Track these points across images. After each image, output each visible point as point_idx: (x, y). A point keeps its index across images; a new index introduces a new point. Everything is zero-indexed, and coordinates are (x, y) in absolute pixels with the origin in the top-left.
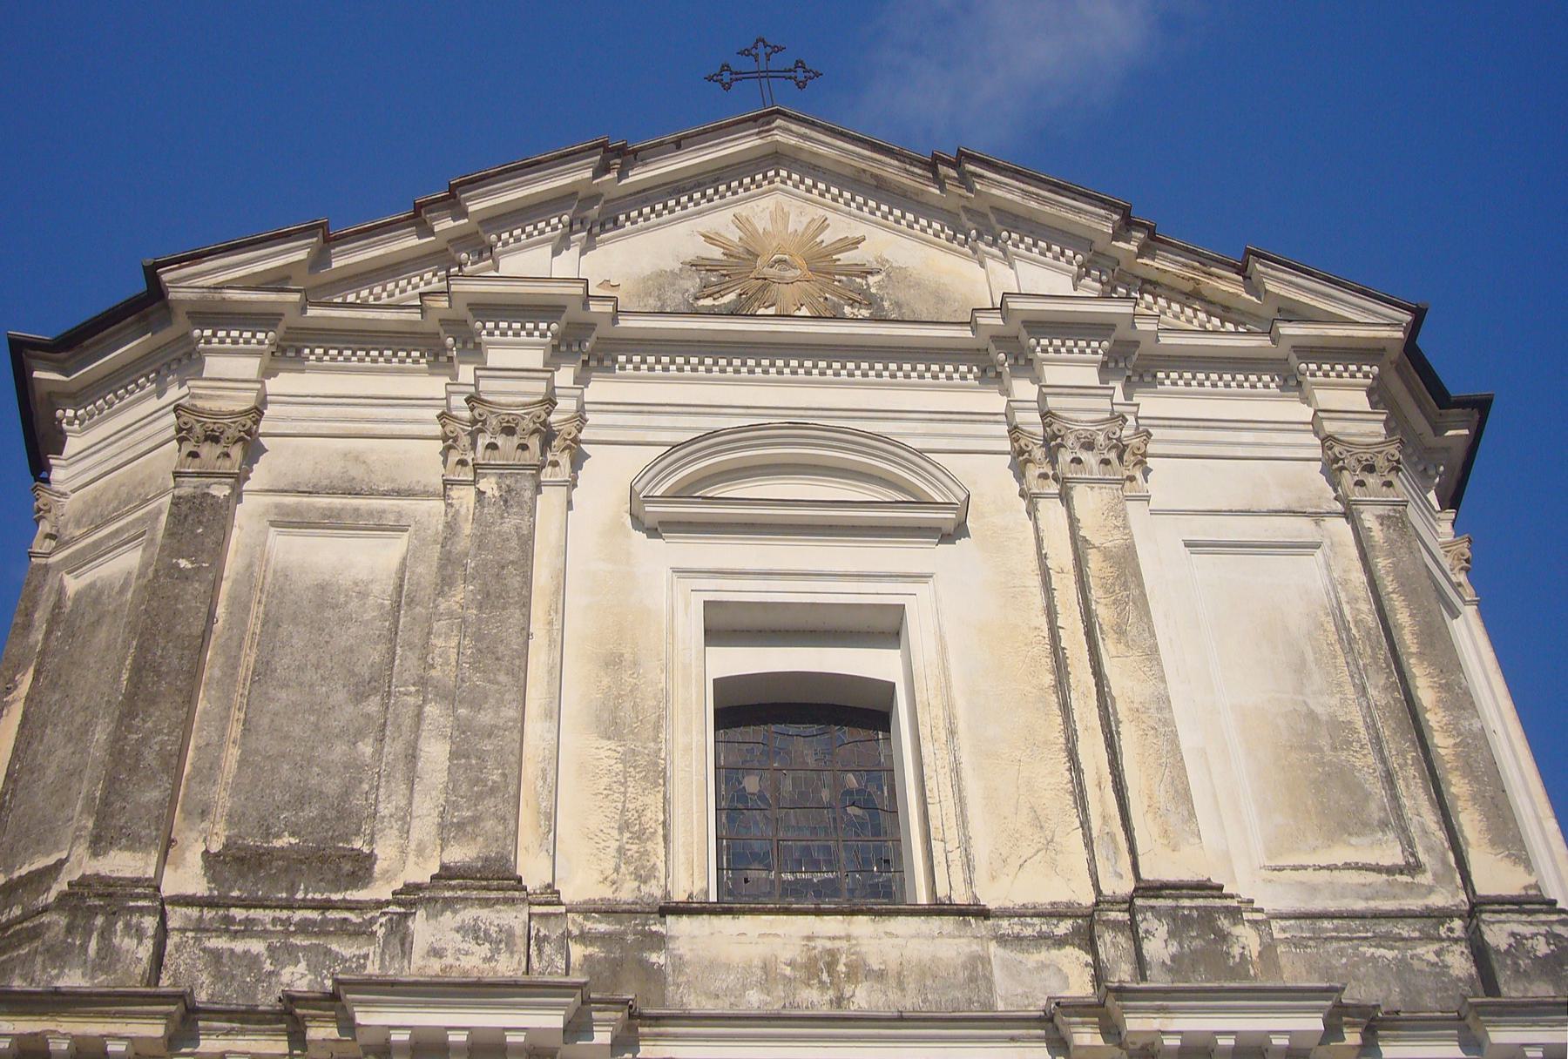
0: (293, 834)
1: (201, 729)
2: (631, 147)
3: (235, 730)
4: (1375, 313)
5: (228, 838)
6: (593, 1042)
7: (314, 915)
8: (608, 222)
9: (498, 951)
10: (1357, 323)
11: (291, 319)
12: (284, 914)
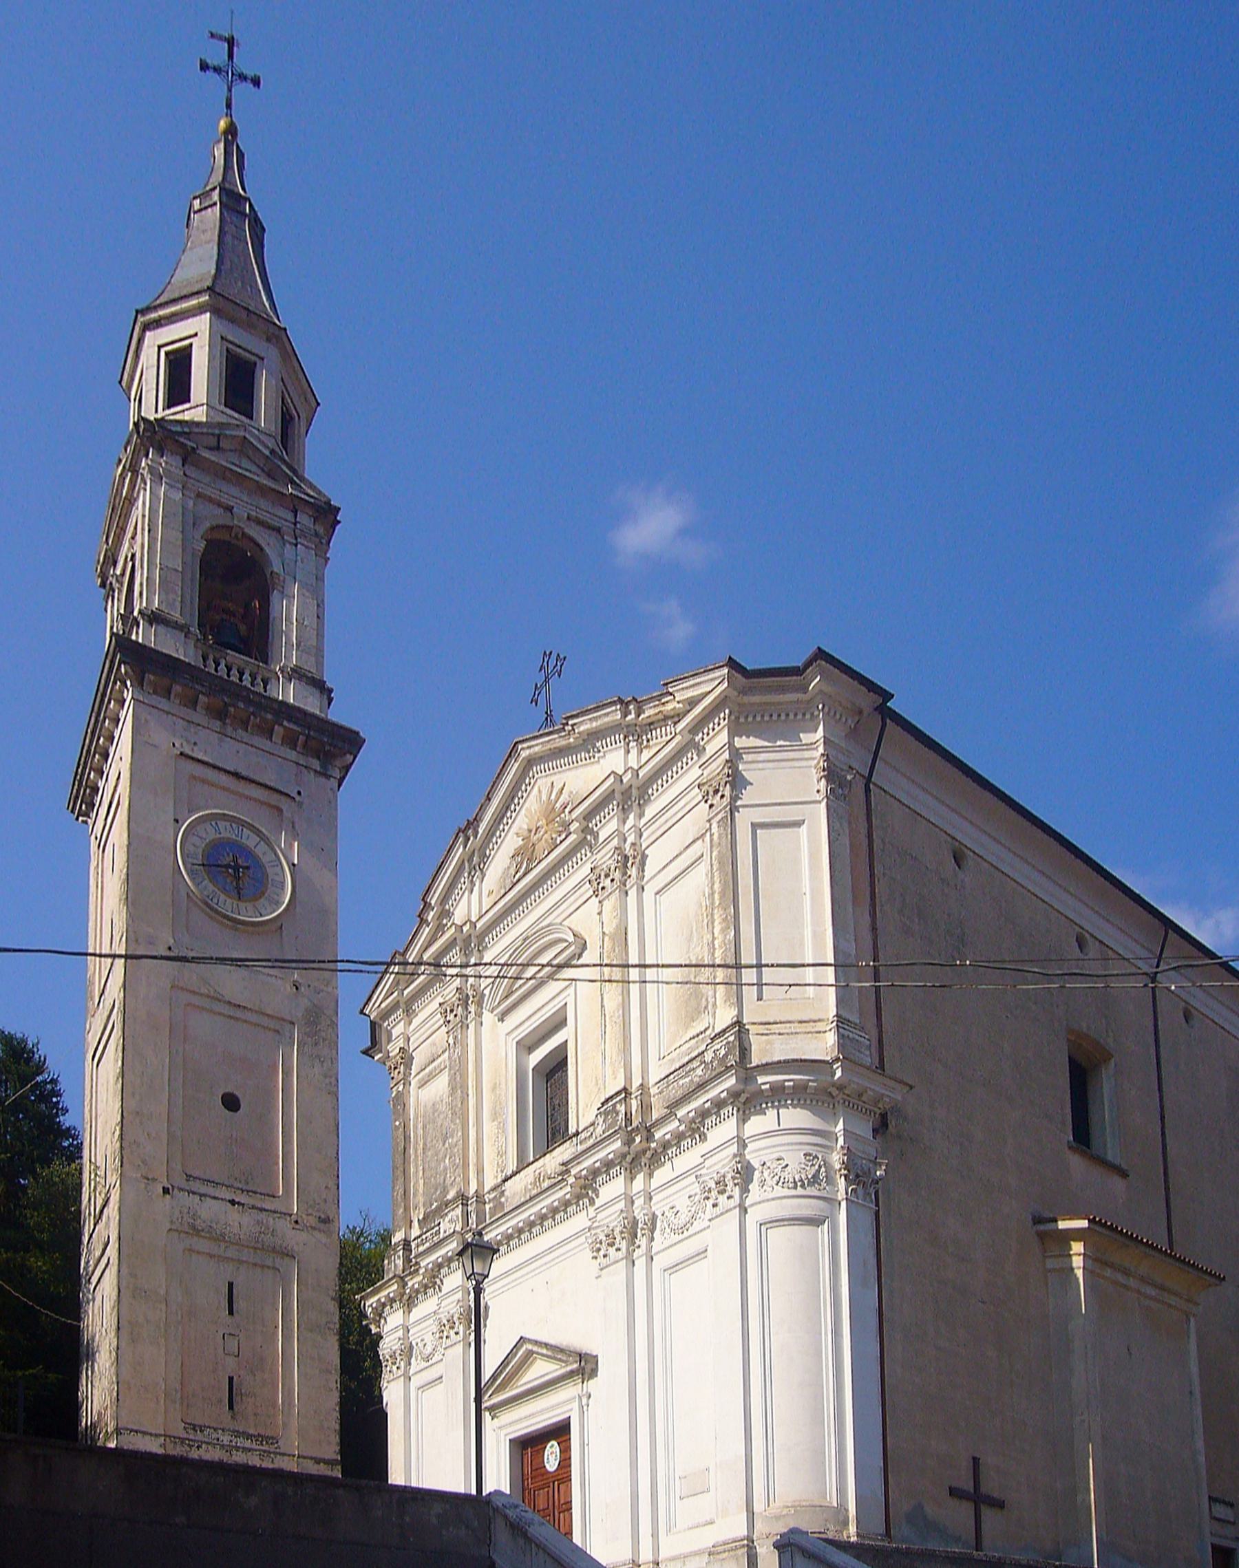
2: (471, 819)
3: (421, 1173)
4: (712, 680)
8: (484, 858)
10: (710, 692)
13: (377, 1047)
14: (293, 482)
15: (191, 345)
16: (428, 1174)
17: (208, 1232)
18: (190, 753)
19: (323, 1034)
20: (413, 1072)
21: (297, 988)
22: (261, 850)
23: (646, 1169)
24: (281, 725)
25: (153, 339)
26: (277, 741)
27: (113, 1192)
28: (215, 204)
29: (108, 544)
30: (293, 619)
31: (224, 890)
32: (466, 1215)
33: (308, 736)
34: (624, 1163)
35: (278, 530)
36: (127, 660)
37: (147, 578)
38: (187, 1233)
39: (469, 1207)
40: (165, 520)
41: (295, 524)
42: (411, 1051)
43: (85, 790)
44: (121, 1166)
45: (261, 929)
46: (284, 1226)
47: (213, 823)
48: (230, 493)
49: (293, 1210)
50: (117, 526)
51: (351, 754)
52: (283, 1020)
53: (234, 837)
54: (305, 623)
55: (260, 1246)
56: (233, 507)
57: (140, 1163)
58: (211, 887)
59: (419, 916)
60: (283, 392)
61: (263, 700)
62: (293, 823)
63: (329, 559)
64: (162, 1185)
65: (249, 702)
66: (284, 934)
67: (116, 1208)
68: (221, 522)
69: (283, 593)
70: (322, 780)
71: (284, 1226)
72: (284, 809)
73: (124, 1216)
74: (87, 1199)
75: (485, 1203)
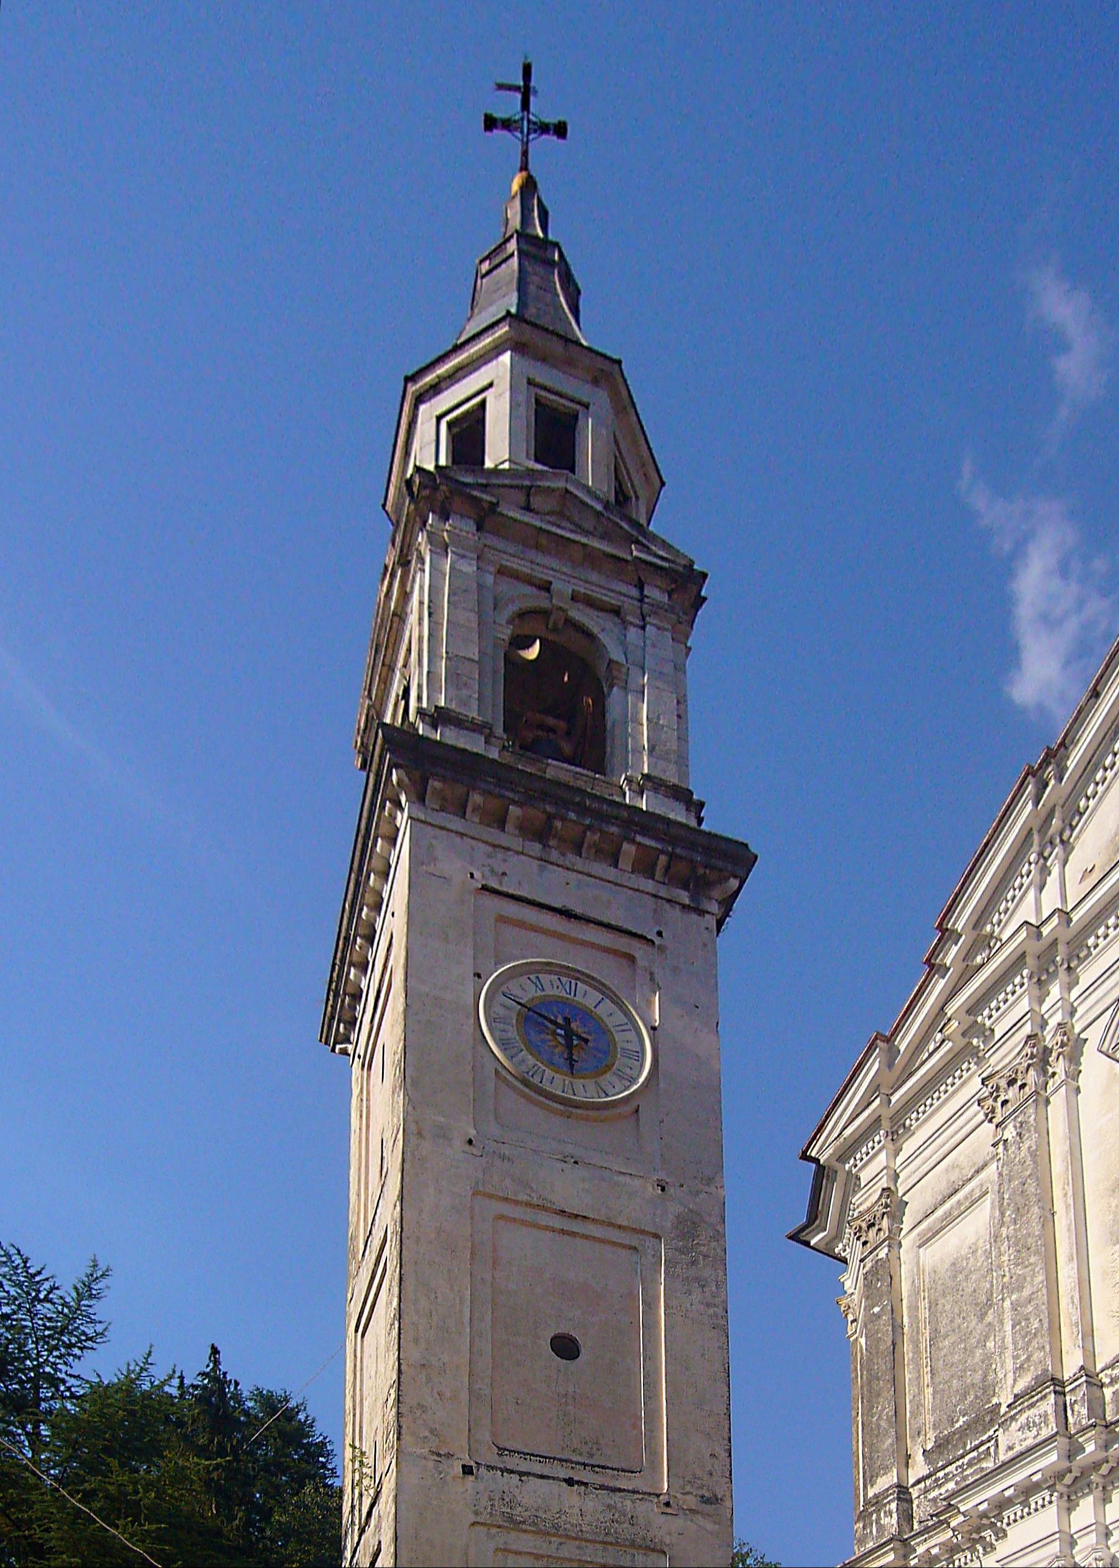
0: (964, 1416)
1: (910, 1391)
3: (927, 1378)
5: (935, 1437)
6: (1087, 1453)
7: (975, 1454)
8: (1073, 814)
9: (1041, 1429)
11: (886, 1113)
12: (959, 1463)
13: (817, 1222)
14: (637, 542)
15: (483, 404)
16: (943, 1375)
17: (535, 1524)
18: (497, 887)
19: (704, 1249)
20: (906, 1227)
21: (663, 1189)
22: (605, 1010)
23: (1098, 1492)
24: (633, 841)
25: (428, 411)
26: (625, 868)
27: (385, 1481)
28: (512, 255)
29: (371, 699)
30: (642, 719)
31: (550, 1063)
32: (1062, 1410)
33: (672, 856)
34: (1058, 1487)
35: (616, 612)
36: (400, 761)
37: (429, 672)
38: (499, 1527)
39: (1068, 1398)
40: (453, 598)
41: (641, 601)
42: (900, 1194)
43: (343, 1001)
44: (398, 1439)
45: (607, 1113)
46: (648, 1510)
47: (533, 977)
48: (547, 566)
49: (663, 1489)
50: (383, 665)
51: (735, 877)
52: (643, 1232)
53: (563, 994)
54: (661, 722)
55: (609, 1539)
56: (551, 583)
57: (427, 1433)
58: (531, 1060)
59: (928, 961)
60: (616, 457)
61: (605, 807)
62: (652, 974)
63: (690, 649)
64: (461, 1463)
65: (583, 810)
66: (642, 1121)
67: (391, 1497)
68: (529, 604)
69: (626, 688)
70: (694, 917)
71: (648, 1510)
72: (638, 955)
73: (403, 1507)
74: (349, 1509)
75: (1102, 1386)
